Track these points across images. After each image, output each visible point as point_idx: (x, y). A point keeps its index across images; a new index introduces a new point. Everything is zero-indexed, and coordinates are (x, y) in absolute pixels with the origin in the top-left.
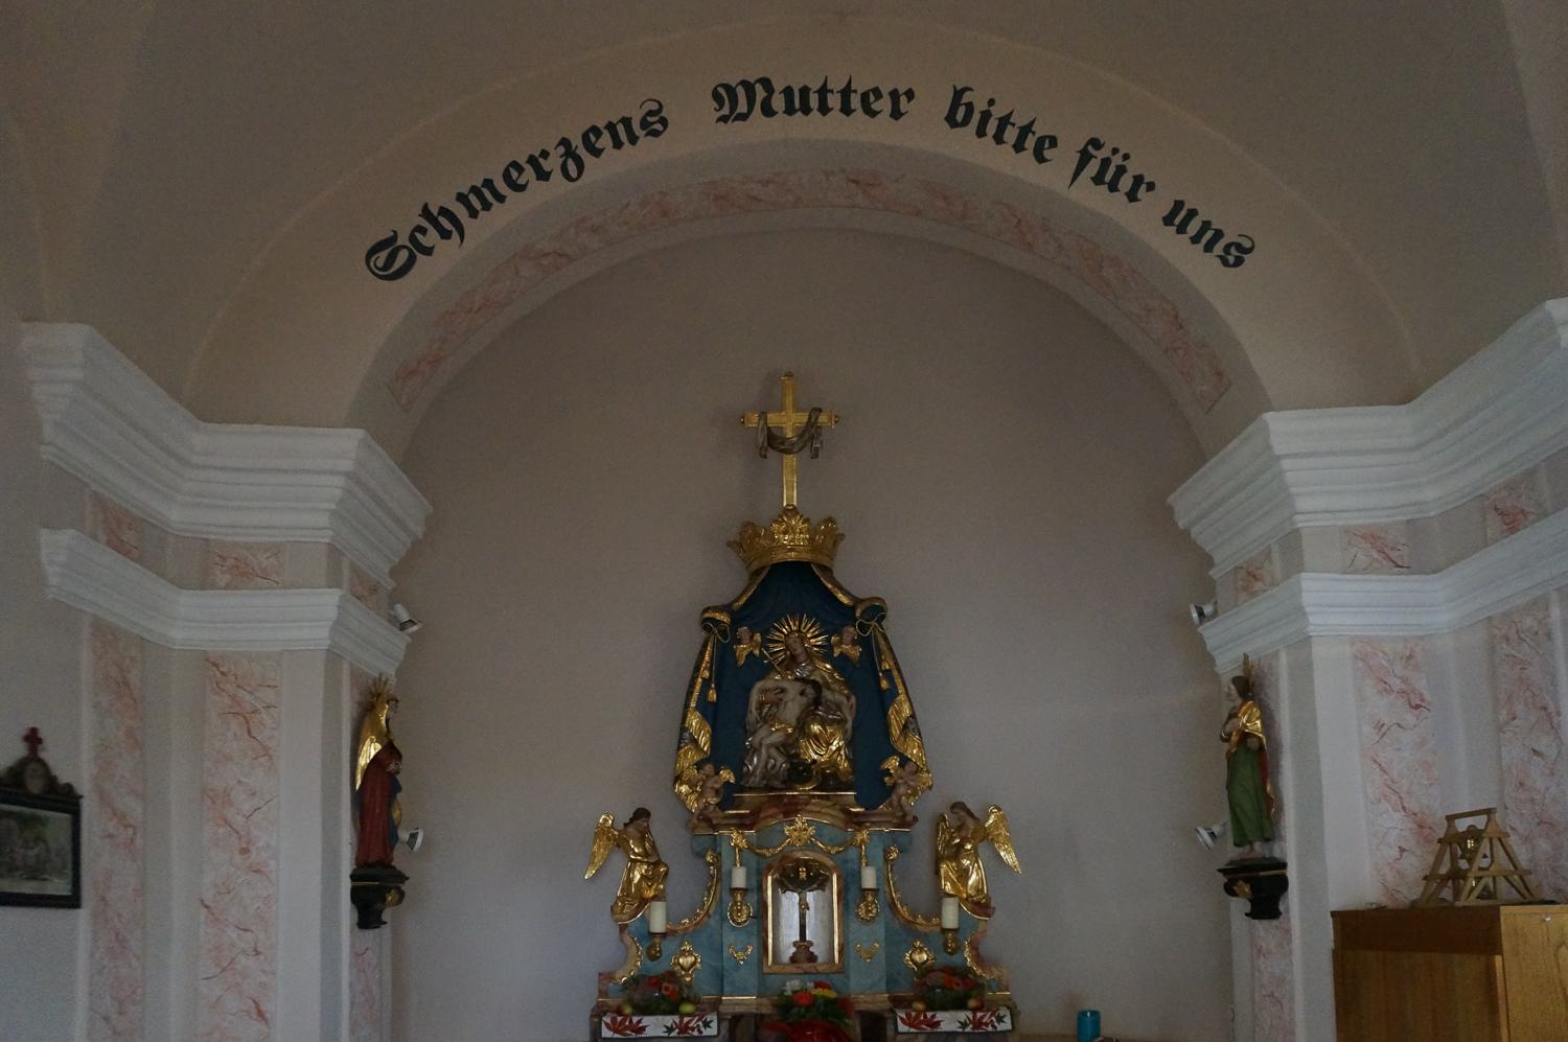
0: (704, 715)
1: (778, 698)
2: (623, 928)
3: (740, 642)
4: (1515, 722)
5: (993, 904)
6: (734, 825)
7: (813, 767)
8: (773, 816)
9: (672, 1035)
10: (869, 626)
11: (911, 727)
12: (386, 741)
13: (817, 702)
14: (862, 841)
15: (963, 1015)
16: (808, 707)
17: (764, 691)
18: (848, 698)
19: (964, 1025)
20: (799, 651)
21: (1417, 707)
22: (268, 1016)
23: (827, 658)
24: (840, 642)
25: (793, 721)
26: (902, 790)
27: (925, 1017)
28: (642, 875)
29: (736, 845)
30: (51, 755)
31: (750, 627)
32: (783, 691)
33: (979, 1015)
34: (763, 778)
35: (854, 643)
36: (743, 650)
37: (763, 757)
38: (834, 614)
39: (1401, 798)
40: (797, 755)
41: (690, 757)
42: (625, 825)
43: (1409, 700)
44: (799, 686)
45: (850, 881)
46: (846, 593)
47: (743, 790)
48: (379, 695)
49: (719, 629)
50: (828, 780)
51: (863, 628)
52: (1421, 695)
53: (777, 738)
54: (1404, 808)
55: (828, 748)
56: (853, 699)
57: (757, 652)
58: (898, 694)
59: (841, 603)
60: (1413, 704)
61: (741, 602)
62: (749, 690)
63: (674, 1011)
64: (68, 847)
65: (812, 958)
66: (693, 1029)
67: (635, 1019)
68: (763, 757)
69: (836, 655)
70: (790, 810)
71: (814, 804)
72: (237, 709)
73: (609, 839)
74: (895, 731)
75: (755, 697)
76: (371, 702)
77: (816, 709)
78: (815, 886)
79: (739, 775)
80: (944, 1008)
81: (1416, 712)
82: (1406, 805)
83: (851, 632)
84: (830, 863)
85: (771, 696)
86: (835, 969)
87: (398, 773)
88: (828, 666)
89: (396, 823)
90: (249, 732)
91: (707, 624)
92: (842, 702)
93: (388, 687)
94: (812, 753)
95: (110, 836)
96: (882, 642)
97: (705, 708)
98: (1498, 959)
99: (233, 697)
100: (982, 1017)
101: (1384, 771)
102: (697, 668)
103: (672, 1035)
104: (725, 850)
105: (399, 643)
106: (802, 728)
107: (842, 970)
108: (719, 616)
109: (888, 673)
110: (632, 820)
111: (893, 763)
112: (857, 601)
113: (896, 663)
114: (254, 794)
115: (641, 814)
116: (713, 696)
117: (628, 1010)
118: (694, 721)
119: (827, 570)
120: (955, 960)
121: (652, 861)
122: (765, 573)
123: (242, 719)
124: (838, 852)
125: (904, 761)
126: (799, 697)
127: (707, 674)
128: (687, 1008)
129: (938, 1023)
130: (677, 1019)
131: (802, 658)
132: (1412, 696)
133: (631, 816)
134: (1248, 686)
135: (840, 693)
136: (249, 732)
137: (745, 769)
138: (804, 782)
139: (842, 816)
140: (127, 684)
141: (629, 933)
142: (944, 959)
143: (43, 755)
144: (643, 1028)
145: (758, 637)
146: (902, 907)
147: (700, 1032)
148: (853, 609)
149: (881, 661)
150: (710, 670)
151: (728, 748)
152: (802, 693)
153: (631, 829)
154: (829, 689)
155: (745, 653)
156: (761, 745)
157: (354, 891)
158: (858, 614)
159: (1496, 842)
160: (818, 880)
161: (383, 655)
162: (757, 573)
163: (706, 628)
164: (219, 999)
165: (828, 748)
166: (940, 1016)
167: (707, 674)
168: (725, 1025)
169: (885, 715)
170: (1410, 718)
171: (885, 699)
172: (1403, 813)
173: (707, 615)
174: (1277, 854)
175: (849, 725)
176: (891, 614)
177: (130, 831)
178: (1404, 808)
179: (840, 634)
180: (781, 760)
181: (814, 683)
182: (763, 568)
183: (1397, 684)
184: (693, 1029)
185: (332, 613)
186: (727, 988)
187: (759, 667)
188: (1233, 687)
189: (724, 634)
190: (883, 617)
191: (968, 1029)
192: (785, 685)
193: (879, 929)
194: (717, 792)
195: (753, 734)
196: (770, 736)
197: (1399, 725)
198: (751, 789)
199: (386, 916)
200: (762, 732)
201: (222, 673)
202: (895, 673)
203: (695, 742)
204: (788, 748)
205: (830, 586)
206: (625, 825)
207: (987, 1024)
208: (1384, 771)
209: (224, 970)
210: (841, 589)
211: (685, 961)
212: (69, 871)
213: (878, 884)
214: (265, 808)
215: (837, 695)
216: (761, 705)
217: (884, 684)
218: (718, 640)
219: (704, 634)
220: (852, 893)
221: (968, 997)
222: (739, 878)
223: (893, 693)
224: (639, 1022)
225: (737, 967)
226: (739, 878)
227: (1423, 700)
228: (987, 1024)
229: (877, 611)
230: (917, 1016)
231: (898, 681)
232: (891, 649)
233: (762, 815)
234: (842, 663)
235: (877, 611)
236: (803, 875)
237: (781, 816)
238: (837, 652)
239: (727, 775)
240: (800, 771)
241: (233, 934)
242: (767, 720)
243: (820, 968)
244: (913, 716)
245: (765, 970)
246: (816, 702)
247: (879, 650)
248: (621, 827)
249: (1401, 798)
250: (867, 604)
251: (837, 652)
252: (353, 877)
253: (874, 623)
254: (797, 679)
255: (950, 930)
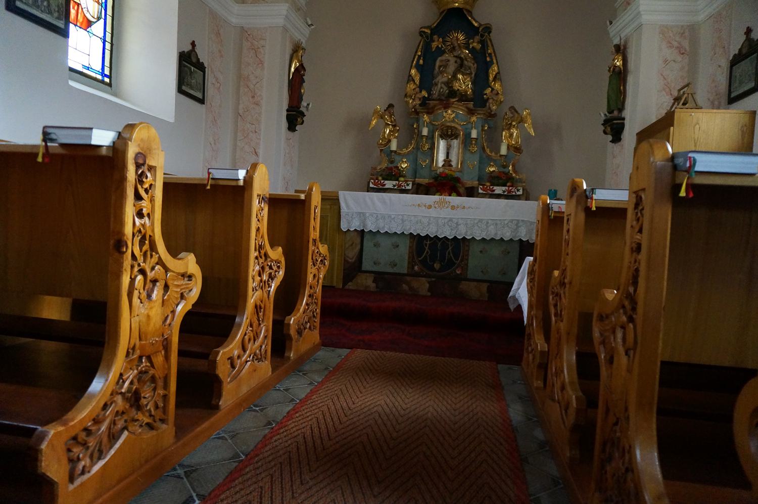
0: (418, 69)
1: (445, 65)
2: (381, 150)
3: (434, 41)
4: (716, 55)
5: (522, 148)
6: (424, 112)
7: (458, 92)
8: (440, 109)
9: (395, 188)
10: (484, 35)
11: (498, 77)
12: (300, 63)
13: (462, 65)
14: (474, 121)
15: (504, 188)
16: (457, 68)
17: (441, 61)
18: (474, 64)
19: (504, 192)
20: (456, 45)
21: (683, 54)
22: (258, 154)
23: (467, 48)
24: (473, 42)
25: (452, 74)
26: (491, 101)
27: (490, 188)
28: (390, 130)
29: (425, 120)
30: (198, 50)
31: (438, 36)
32: (449, 61)
33: (510, 188)
34: (439, 96)
35: (478, 43)
36: (434, 45)
37: (439, 88)
38: (472, 31)
39: (670, 90)
40: (452, 87)
41: (412, 86)
42: (385, 110)
43: (680, 51)
44: (455, 59)
45: (468, 135)
46: (476, 22)
47: (430, 100)
48: (299, 47)
49: (427, 36)
50: (463, 98)
51: (482, 36)
52: (685, 49)
53: (445, 79)
54: (671, 94)
55: (464, 84)
56: (475, 65)
57: (440, 46)
58: (493, 64)
59: (474, 26)
60: (682, 52)
61: (435, 25)
62: (435, 60)
63: (397, 180)
64: (202, 83)
65: (451, 166)
66: (403, 186)
67: (382, 181)
68: (439, 88)
69: (471, 47)
70: (446, 107)
71: (455, 104)
72: (253, 47)
73: (378, 115)
74: (491, 78)
75: (438, 63)
76: (297, 49)
77: (461, 68)
78: (536, 267)
79: (429, 94)
80: (498, 185)
81: (682, 56)
82: (672, 93)
83: (477, 38)
84: (459, 128)
85: (444, 63)
86: (458, 170)
87: (304, 75)
88: (467, 52)
89: (302, 93)
90: (256, 55)
91: (422, 34)
92: (471, 66)
93: (302, 45)
94: (456, 86)
95: (213, 84)
96: (489, 42)
97: (418, 67)
98: (672, 128)
99: (252, 43)
100: (512, 189)
101: (665, 79)
102: (416, 52)
103: (395, 188)
104: (421, 123)
105: (307, 31)
106: (454, 77)
107: (460, 171)
108: (426, 31)
109: (490, 55)
110: (387, 108)
111: (488, 91)
112: (480, 25)
113: (494, 51)
114: (257, 77)
115: (391, 106)
116: (421, 62)
117: (380, 178)
118: (413, 72)
119: (470, 12)
120: (506, 170)
121: (393, 124)
122: (445, 12)
123: (254, 51)
124: (463, 125)
125: (493, 90)
126: (454, 64)
127: (420, 53)
128: (402, 179)
129: (494, 191)
130: (397, 182)
131: (457, 48)
132: (681, 49)
133: (387, 106)
134: (621, 50)
135: (471, 62)
136: (256, 55)
137: (432, 92)
138: (455, 97)
139: (466, 109)
140: (219, 34)
141: (384, 152)
142: (502, 170)
143: (196, 50)
144: (385, 185)
145: (441, 40)
146: (487, 148)
147: (405, 187)
148: (478, 28)
149: (488, 49)
150: (421, 52)
151: (426, 82)
152: (456, 62)
153: (387, 112)
154: (466, 60)
155: (435, 46)
156: (438, 82)
157: (287, 116)
158: (480, 30)
159: (690, 95)
160: (456, 136)
161: (302, 34)
162: (443, 12)
163: (421, 35)
164: (243, 147)
165: (464, 84)
166: (495, 188)
167: (420, 53)
168: (415, 186)
169: (488, 70)
170: (679, 58)
171: (488, 65)
172: (670, 96)
173: (421, 30)
174: (623, 116)
175: (473, 75)
176: (493, 31)
177: (219, 85)
178: (671, 94)
179: (473, 39)
180: (445, 88)
181: (461, 58)
182: (444, 11)
183: (676, 44)
184: (403, 186)
185: (285, 13)
186: (417, 176)
187: (440, 52)
188: (613, 48)
189: (427, 37)
190: (490, 32)
191: (505, 193)
192: (450, 58)
193: (477, 157)
194: (420, 99)
195: (436, 79)
196: (441, 79)
197: (674, 61)
198: (433, 100)
199: (297, 128)
200: (440, 77)
201: (248, 35)
202: (493, 55)
203: (414, 81)
204: (448, 84)
205: (470, 18)
206: (385, 110)
207: (513, 192)
208: (665, 79)
209: (245, 137)
210: (474, 20)
211: (404, 166)
212: (202, 91)
213: (478, 136)
214: (260, 82)
215: (470, 63)
216: (440, 67)
217: (488, 59)
218: (425, 40)
219: (420, 38)
220: (467, 141)
221: (506, 183)
222: (425, 132)
223: (491, 63)
224: (384, 182)
225: (422, 168)
226: (425, 132)
227: (686, 51)
228: (513, 192)
229: (488, 29)
230: (487, 187)
231: (494, 58)
232: (492, 45)
233: (436, 108)
234: (473, 51)
235: (488, 29)
236: (449, 133)
237: (443, 109)
238: (471, 46)
239: (424, 94)
240: (453, 93)
241: (248, 125)
242: (441, 72)
243: (453, 169)
244: (498, 73)
245: (432, 169)
246: (461, 67)
247: (487, 44)
248: (383, 111)
249: (670, 90)
250: (484, 26)
251: (471, 46)
252: (287, 111)
253: (486, 34)
254: (454, 56)
255: (503, 155)
